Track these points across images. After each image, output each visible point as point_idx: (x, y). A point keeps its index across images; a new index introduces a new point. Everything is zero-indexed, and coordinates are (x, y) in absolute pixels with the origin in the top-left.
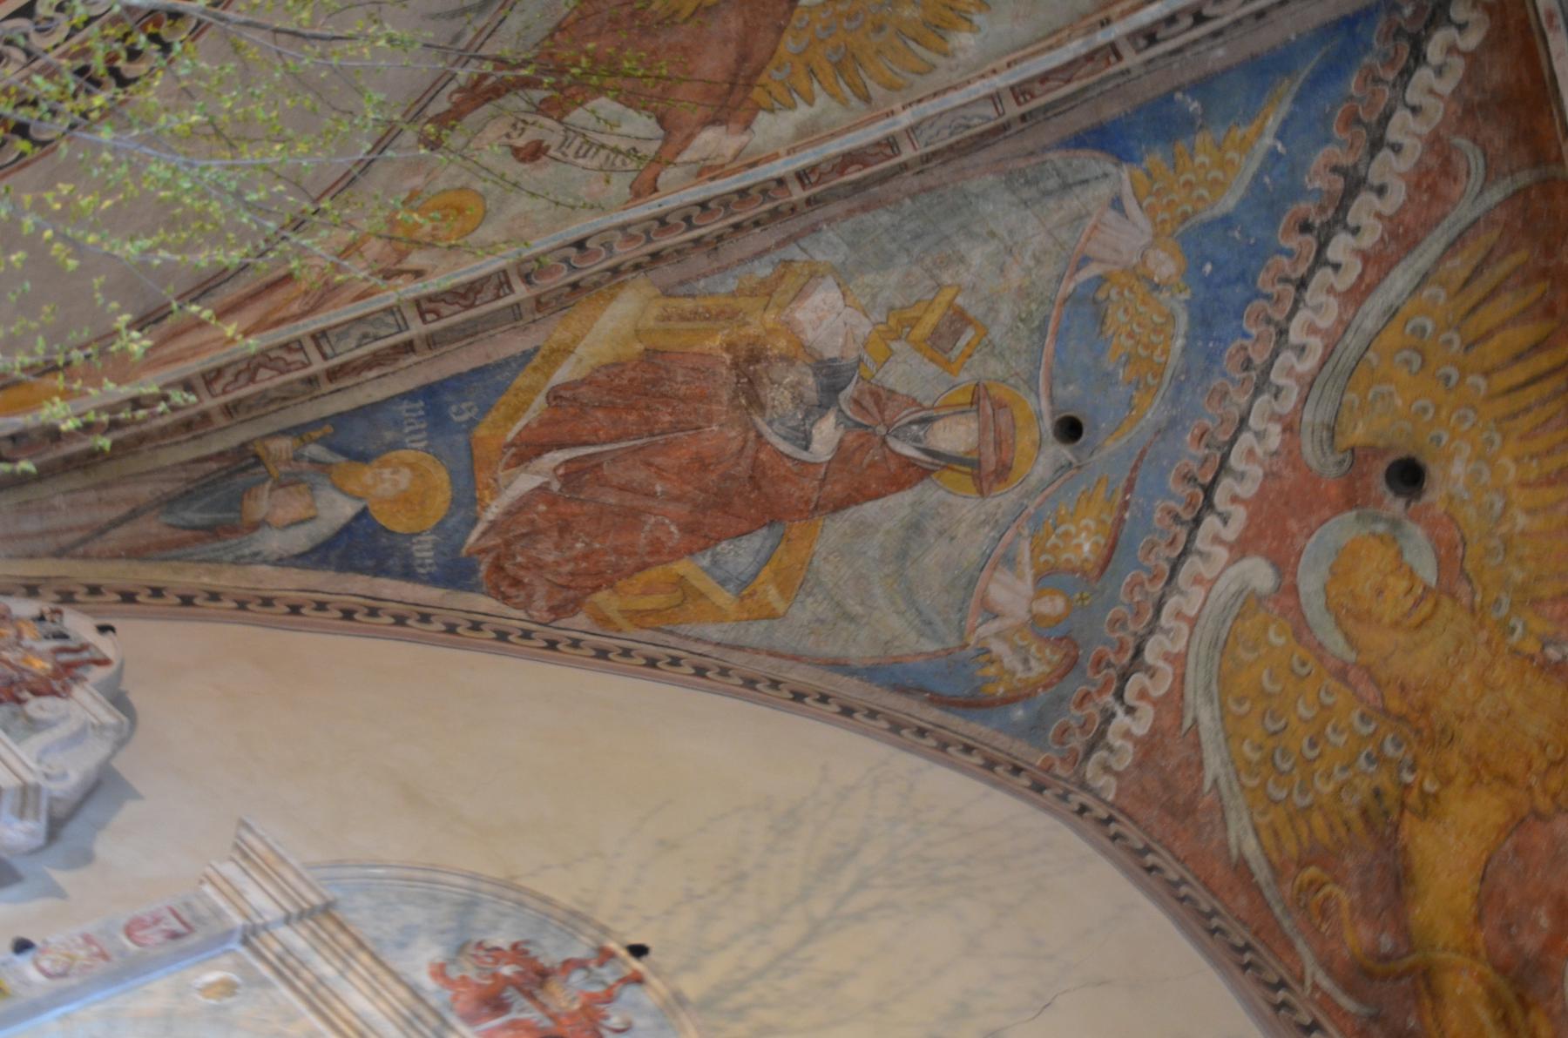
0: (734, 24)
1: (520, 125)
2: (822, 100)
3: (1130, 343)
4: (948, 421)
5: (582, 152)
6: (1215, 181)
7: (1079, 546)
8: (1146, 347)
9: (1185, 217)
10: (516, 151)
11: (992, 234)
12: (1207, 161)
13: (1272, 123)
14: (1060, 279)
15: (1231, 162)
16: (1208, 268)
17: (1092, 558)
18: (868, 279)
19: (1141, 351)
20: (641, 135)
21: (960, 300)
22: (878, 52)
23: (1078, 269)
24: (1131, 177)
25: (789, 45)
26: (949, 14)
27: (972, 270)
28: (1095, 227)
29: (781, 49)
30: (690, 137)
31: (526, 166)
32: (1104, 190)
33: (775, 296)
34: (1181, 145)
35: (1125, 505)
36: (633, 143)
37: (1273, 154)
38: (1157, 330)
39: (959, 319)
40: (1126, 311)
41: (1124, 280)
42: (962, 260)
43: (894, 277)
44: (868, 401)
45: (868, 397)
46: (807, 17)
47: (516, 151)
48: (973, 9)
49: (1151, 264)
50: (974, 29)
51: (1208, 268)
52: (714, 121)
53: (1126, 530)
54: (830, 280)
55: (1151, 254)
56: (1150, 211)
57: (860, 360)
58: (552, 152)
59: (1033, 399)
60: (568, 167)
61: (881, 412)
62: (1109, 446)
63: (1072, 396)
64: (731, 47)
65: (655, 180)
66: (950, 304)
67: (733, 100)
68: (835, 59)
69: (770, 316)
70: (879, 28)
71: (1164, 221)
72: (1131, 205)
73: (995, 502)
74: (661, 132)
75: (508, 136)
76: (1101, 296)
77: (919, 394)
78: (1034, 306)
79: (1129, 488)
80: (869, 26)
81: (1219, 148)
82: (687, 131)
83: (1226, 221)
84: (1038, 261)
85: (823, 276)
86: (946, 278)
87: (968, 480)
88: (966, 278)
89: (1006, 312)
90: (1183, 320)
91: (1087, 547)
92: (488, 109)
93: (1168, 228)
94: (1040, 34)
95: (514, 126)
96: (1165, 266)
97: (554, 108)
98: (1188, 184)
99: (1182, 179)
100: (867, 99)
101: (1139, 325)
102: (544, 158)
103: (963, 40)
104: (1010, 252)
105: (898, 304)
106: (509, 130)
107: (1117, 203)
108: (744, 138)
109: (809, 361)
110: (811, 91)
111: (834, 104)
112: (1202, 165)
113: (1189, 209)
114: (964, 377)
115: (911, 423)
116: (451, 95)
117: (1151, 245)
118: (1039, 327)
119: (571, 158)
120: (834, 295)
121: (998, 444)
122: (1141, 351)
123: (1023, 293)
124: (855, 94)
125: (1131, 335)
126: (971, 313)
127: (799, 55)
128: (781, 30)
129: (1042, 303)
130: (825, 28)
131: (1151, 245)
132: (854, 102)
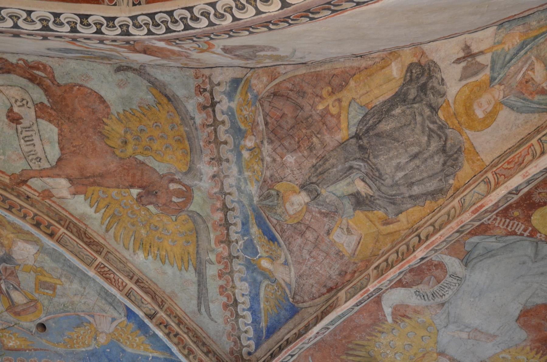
0: (113, 166)
1: (24, 102)
2: (99, 215)
3: (76, 338)
4: (21, 294)
5: (27, 139)
6: (133, 345)
7: (10, 342)
8: (77, 342)
9: (119, 340)
10: (11, 110)
11: (85, 288)
12: (138, 341)
13: (155, 354)
14: (83, 311)
15: (140, 347)
16: (108, 350)
17: (9, 346)
18: (47, 258)
19: (75, 341)
20: (49, 157)
21: (58, 286)
22: (125, 228)
23: (89, 315)
24: (124, 321)
25: (114, 192)
26: (148, 247)
27: (70, 286)
28: (104, 316)
29: (111, 190)
30: (59, 176)
31: (6, 120)
32: (116, 315)
33: (20, 234)
34: (139, 332)
35: (30, 350)
36: (43, 157)
37: (148, 357)
38: (83, 343)
39: (54, 288)
40: (84, 333)
41: (93, 329)
42: (71, 282)
43: (53, 265)
44: (9, 272)
45: (10, 271)
46: (127, 194)
47: (11, 110)
48: (153, 254)
49: (101, 335)
50: (146, 258)
51: (108, 350)
52: (70, 180)
53: (23, 352)
54: (38, 247)
55: (104, 334)
56: (116, 329)
57: (20, 265)
58: (19, 127)
59: (44, 315)
60: (16, 138)
61: (9, 275)
62: (42, 341)
63: (51, 325)
64: (104, 169)
65: (31, 178)
66: (56, 284)
67: (82, 182)
68: (116, 213)
69: (12, 236)
70: (133, 225)
71: (115, 335)
72: (115, 323)
73: (7, 314)
74: (54, 164)
75: (16, 101)
76: (85, 324)
77: (22, 284)
78: (70, 307)
79: (35, 350)
80: (132, 221)
81: (143, 343)
82: (61, 173)
83: (123, 351)
84: (85, 303)
85: (37, 245)
86: (63, 279)
87: (8, 305)
88: (67, 286)
89: (63, 300)
90: (90, 348)
91: (11, 344)
92: (24, 82)
93: (114, 336)
94: (153, 280)
95: (23, 100)
96: (102, 339)
97: (41, 110)
98: (129, 338)
99: (129, 336)
100: (107, 231)
101: (82, 338)
102: (14, 125)
103: (141, 255)
104: (82, 295)
105: (45, 269)
106: (20, 100)
107: (114, 320)
108: (69, 197)
109: (7, 251)
110: (100, 210)
111: (100, 221)
112: (136, 340)
113: (122, 341)
114: (37, 295)
115: (12, 285)
116: (20, 60)
117: (106, 334)
118: (65, 311)
119: (21, 136)
120: (35, 251)
121: (24, 310)
122: (75, 341)
123: (73, 303)
124: (107, 225)
125: (78, 337)
126: (57, 291)
127: (112, 197)
128: (118, 187)
129: (73, 309)
130: (125, 204)
131: (106, 334)
132: (104, 227)
